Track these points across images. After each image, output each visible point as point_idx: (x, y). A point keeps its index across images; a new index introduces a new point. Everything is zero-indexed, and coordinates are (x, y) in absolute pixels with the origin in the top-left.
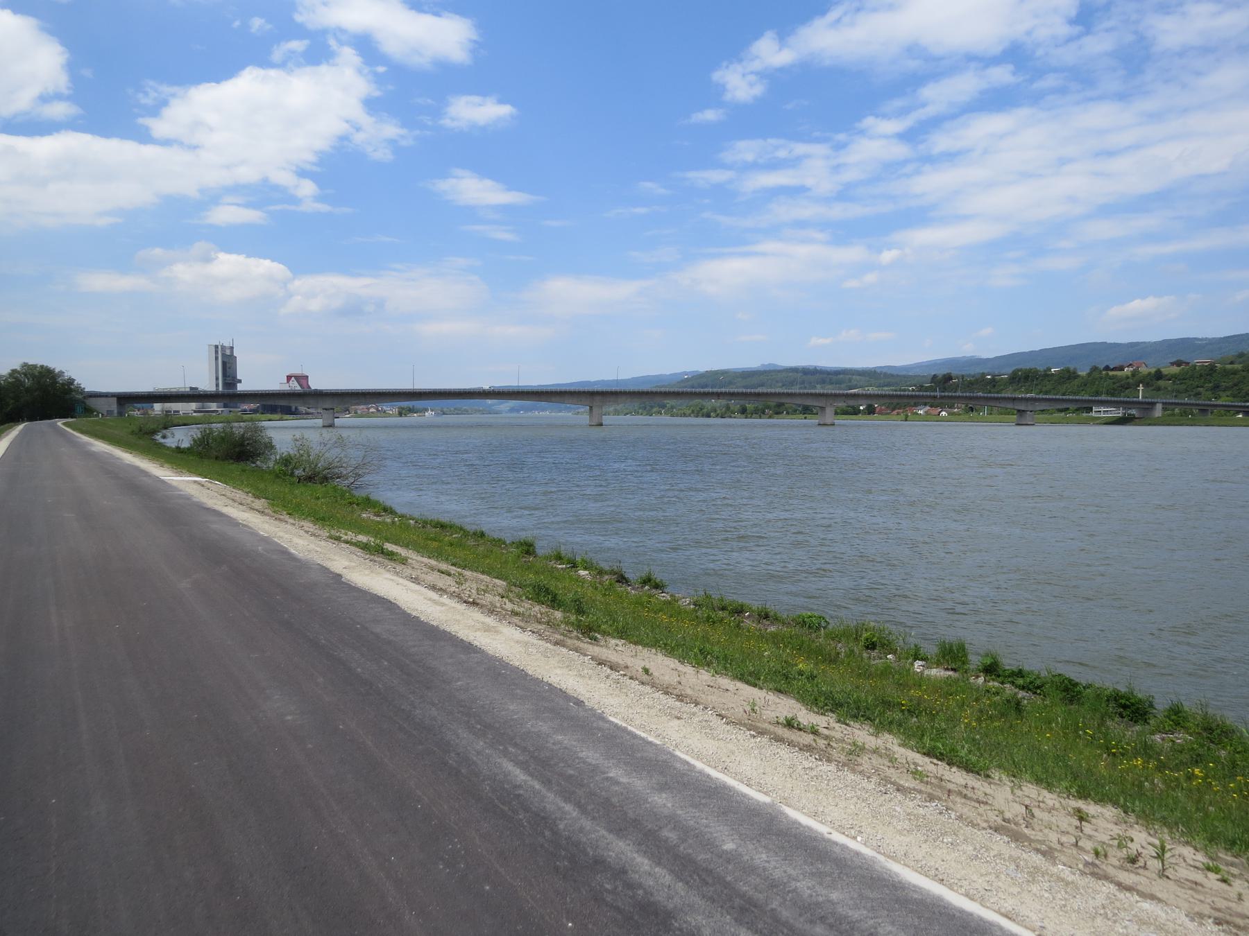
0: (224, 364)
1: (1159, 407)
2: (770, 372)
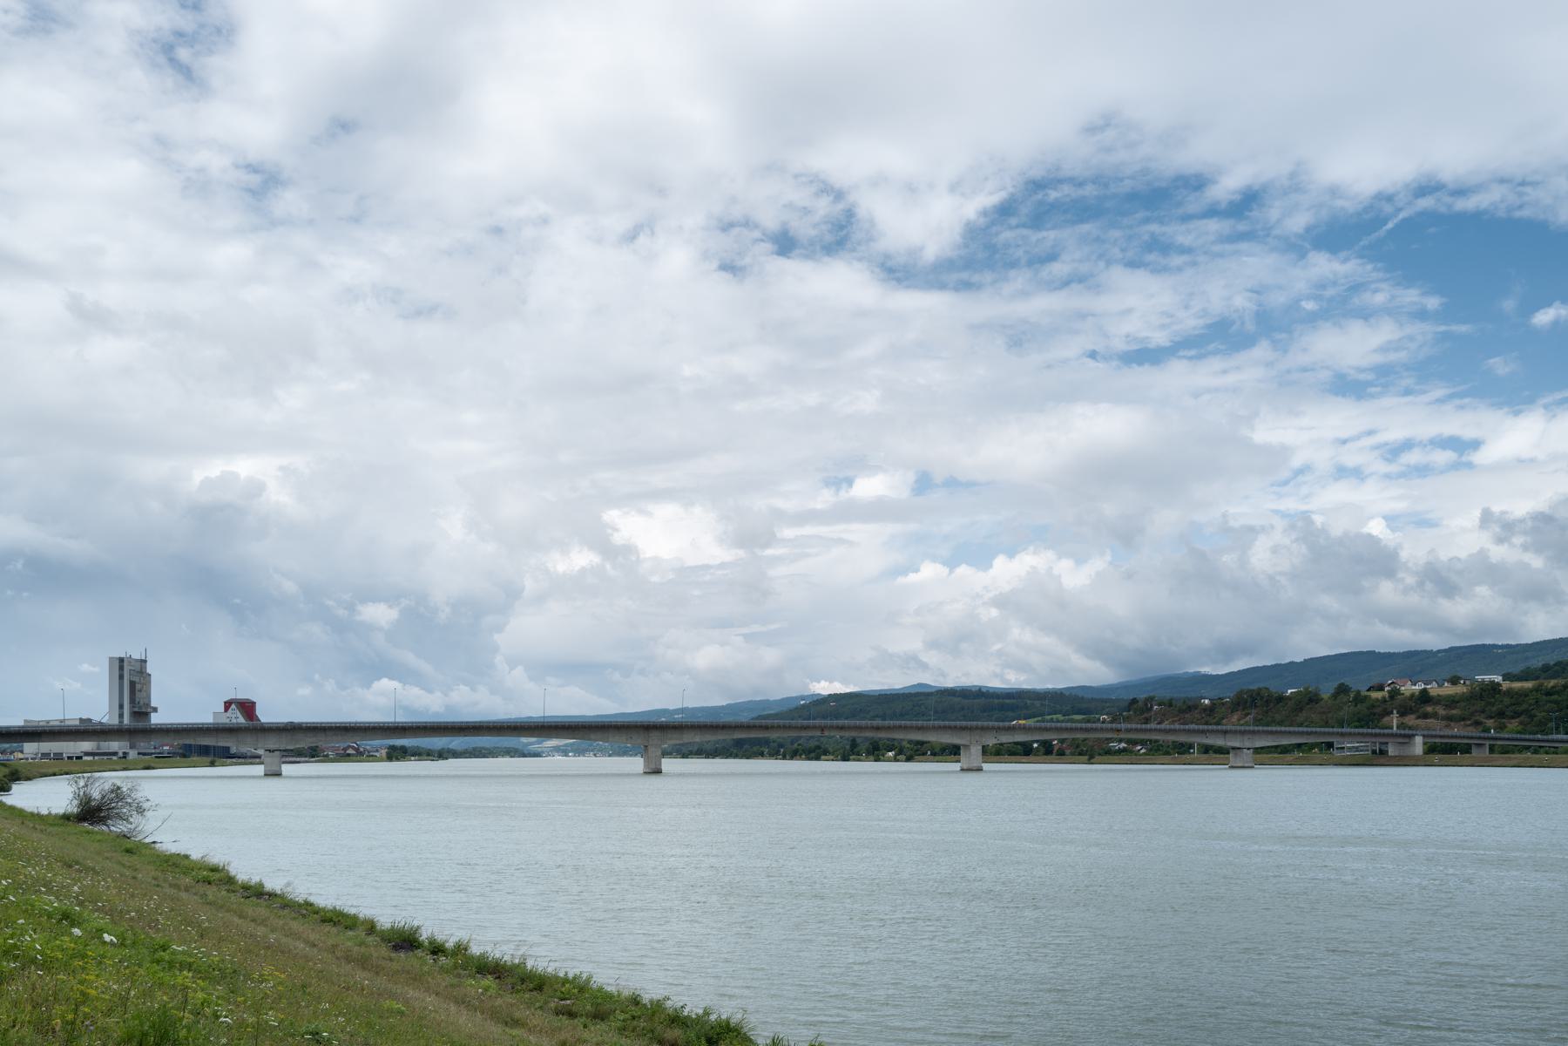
0: (132, 684)
1: (1419, 740)
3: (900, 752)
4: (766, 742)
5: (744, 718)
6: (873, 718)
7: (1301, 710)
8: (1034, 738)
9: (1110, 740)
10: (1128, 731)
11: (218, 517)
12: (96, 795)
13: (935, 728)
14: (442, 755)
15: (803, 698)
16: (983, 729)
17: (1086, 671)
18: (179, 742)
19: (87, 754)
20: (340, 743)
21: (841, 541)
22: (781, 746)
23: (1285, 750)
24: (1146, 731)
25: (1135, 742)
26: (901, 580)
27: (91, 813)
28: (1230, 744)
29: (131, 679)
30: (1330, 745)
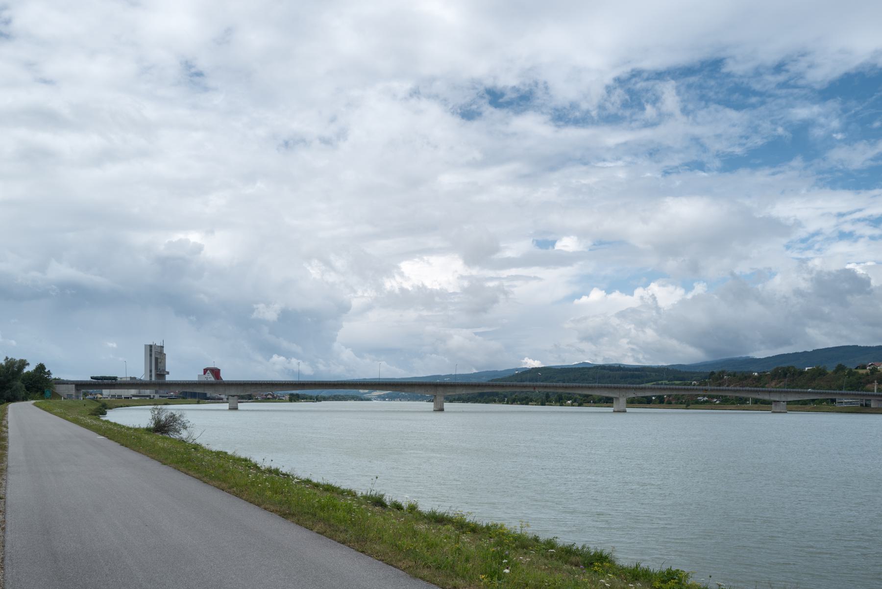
0: (156, 359)
2: (583, 368)
3: (575, 401)
4: (497, 394)
5: (484, 380)
6: (558, 381)
7: (814, 379)
8: (653, 395)
9: (698, 395)
10: (712, 390)
11: (174, 265)
12: (163, 418)
13: (599, 388)
14: (318, 399)
15: (517, 370)
16: (627, 388)
17: (686, 354)
18: (178, 391)
19: (134, 396)
20: (268, 392)
21: (535, 278)
22: (505, 396)
23: (805, 403)
24: (720, 390)
25: (713, 397)
26: (576, 301)
27: (161, 428)
28: (773, 399)
29: (156, 356)
30: (833, 401)
